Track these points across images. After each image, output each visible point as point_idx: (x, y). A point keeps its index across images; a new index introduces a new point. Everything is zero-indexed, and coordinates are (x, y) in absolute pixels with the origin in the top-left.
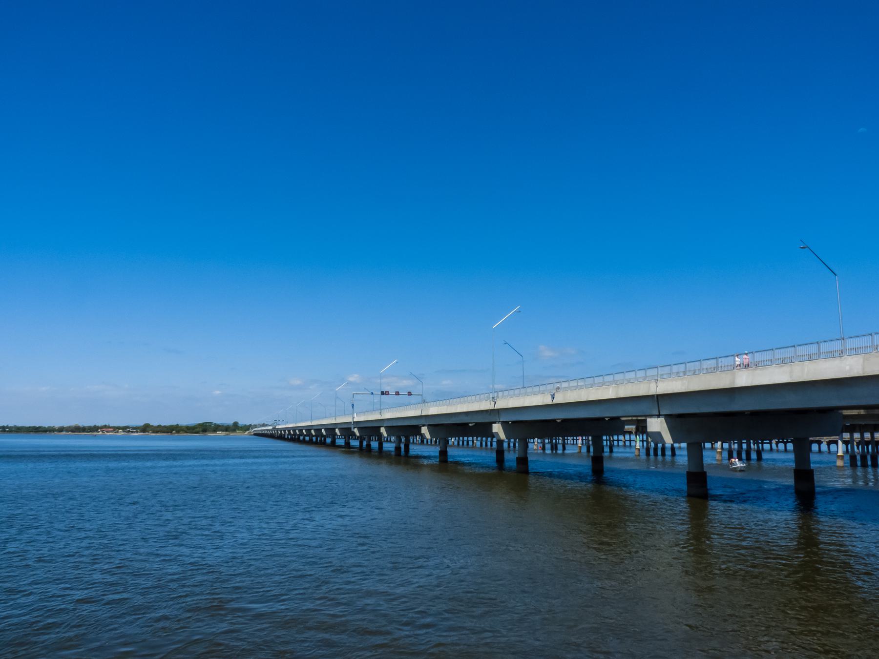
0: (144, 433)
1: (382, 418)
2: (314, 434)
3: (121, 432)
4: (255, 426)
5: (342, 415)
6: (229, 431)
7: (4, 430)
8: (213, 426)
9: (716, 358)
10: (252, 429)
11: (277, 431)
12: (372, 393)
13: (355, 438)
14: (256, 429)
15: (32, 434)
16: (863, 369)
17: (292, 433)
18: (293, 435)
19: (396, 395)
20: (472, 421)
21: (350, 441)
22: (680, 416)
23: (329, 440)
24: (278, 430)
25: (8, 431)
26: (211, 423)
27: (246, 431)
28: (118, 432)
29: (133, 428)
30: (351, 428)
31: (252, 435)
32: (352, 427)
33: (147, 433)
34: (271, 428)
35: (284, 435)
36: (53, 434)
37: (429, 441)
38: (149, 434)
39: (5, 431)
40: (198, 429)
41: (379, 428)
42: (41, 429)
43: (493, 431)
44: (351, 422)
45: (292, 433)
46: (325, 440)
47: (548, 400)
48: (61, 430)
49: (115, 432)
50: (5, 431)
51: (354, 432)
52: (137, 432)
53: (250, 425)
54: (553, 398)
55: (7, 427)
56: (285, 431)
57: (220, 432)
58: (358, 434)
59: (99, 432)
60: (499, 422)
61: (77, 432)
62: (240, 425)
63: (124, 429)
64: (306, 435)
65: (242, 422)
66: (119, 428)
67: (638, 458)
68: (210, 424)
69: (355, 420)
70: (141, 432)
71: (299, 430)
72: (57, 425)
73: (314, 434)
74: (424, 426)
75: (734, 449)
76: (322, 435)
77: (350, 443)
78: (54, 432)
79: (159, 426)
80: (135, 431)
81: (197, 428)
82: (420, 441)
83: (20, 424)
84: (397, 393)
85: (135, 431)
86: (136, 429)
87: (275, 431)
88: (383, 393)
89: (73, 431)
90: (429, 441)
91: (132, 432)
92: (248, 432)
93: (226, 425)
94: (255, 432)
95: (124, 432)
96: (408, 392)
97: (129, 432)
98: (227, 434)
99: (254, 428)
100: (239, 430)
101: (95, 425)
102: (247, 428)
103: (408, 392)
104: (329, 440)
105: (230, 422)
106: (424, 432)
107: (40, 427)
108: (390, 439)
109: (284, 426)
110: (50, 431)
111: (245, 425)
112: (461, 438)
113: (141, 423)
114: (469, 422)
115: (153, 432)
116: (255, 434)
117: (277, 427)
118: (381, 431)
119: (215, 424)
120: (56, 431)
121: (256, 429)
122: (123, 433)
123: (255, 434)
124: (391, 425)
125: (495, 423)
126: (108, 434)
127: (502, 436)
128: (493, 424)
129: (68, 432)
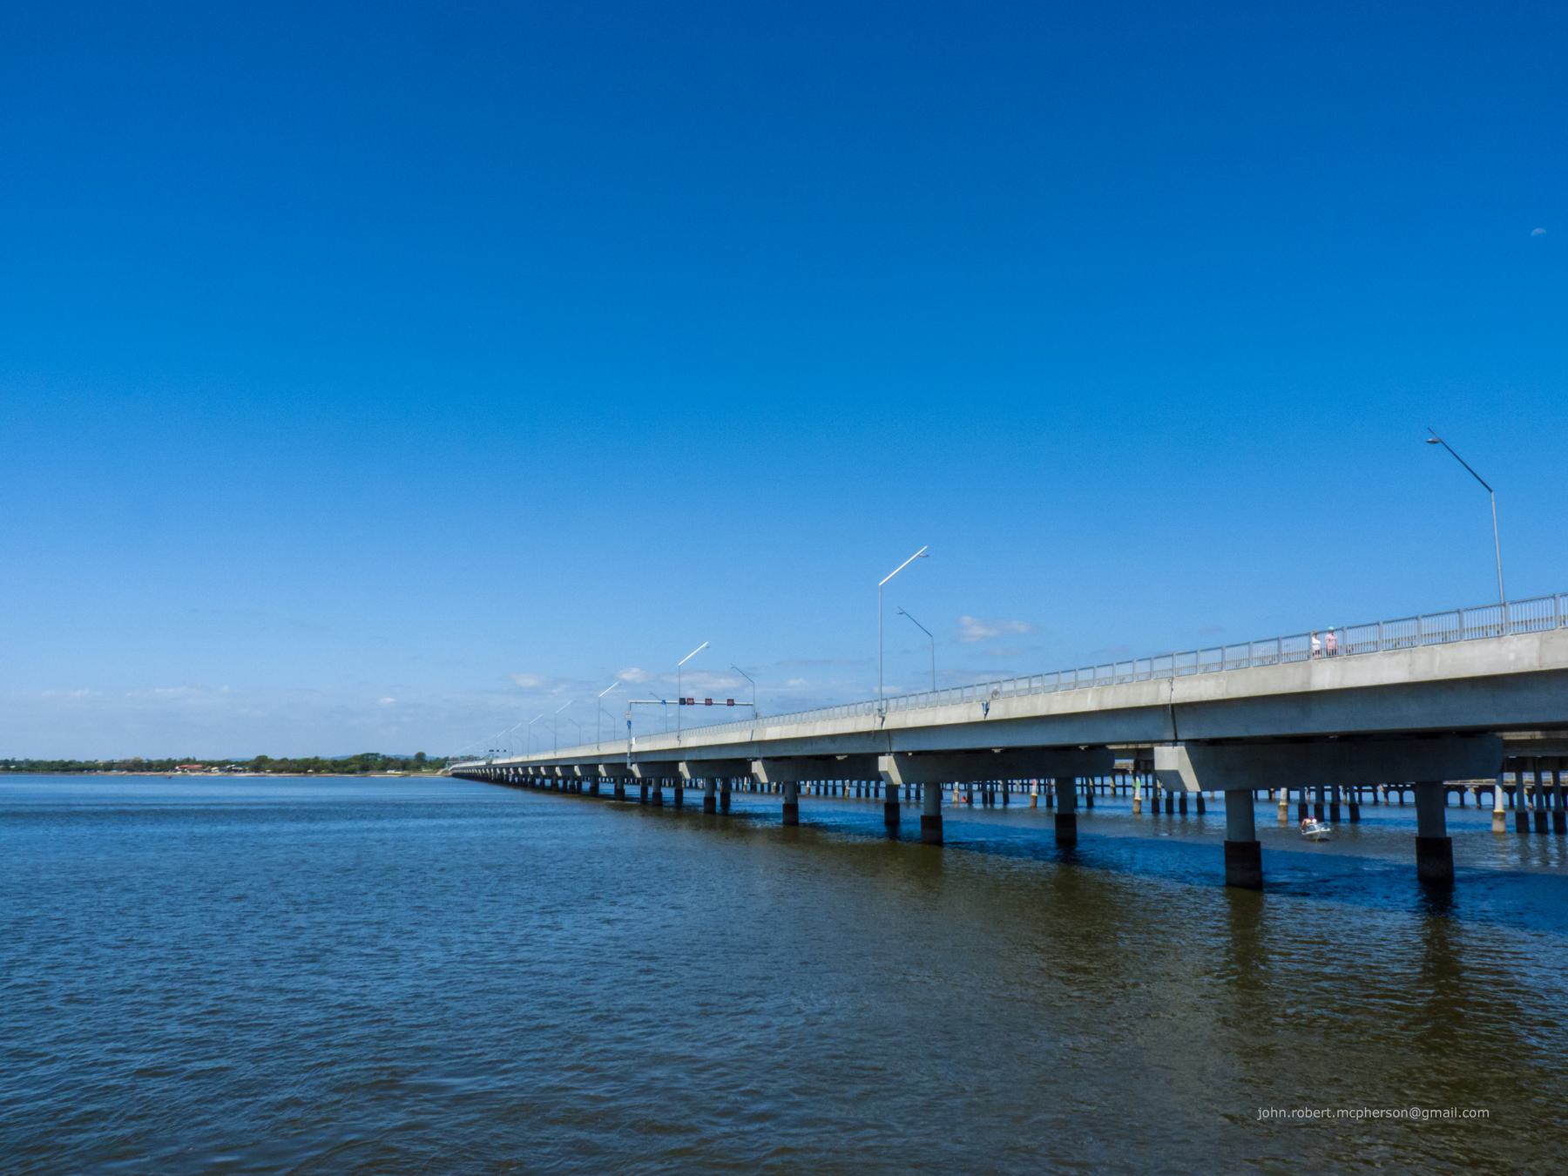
0: (256, 772)
1: (681, 746)
2: (560, 774)
3: (215, 771)
4: (455, 760)
5: (611, 741)
6: (408, 770)
7: (7, 767)
8: (379, 759)
9: (1278, 639)
10: (450, 765)
11: (495, 769)
12: (664, 702)
13: (634, 781)
14: (456, 766)
15: (57, 775)
16: (1540, 658)
17: (531, 772)
18: (523, 776)
19: (706, 704)
20: (842, 751)
21: (625, 787)
22: (1214, 742)
23: (586, 786)
24: (495, 767)
25: (14, 770)
26: (377, 755)
27: (438, 768)
28: (210, 771)
29: (238, 764)
30: (625, 764)
31: (447, 776)
32: (628, 761)
33: (262, 774)
34: (483, 763)
35: (507, 776)
36: (94, 774)
37: (766, 787)
38: (266, 774)
39: (9, 769)
40: (353, 766)
41: (555, 767)
42: (72, 766)
43: (1524, 773)
44: (626, 754)
45: (531, 772)
46: (580, 784)
47: (977, 715)
48: (109, 767)
49: (206, 772)
50: (9, 769)
51: (631, 771)
52: (244, 771)
53: (447, 759)
54: (987, 710)
55: (13, 762)
56: (508, 769)
57: (393, 772)
58: (638, 775)
59: (177, 771)
60: (890, 753)
61: (137, 771)
62: (426, 759)
63: (222, 765)
64: (545, 777)
65: (432, 753)
66: (212, 764)
67: (1139, 817)
68: (374, 756)
69: (634, 749)
70: (252, 770)
71: (534, 768)
72: (102, 759)
73: (560, 774)
74: (756, 759)
75: (1310, 802)
76: (575, 777)
77: (623, 791)
78: (96, 771)
79: (284, 761)
80: (240, 768)
81: (351, 764)
82: (749, 788)
83: (35, 757)
84: (709, 702)
85: (240, 768)
86: (243, 765)
87: (490, 769)
88: (683, 702)
89: (130, 770)
90: (766, 787)
91: (236, 771)
92: (441, 771)
93: (402, 758)
94: (456, 771)
95: (220, 770)
96: (728, 700)
97: (230, 770)
98: (406, 775)
99: (454, 764)
100: (426, 767)
101: (170, 759)
102: (440, 764)
103: (728, 700)
104: (586, 786)
105: (408, 751)
106: (756, 771)
107: (71, 763)
108: (696, 783)
109: (506, 761)
110: (89, 769)
111: (438, 758)
112: (823, 782)
113: (250, 755)
114: (837, 752)
115: (274, 771)
116: (455, 775)
117: (494, 762)
118: (680, 770)
119: (384, 756)
120: (100, 769)
121: (456, 766)
122: (219, 773)
123: (455, 775)
124: (698, 759)
125: (883, 754)
126: (193, 774)
127: (896, 778)
128: (880, 758)
129: (122, 770)
